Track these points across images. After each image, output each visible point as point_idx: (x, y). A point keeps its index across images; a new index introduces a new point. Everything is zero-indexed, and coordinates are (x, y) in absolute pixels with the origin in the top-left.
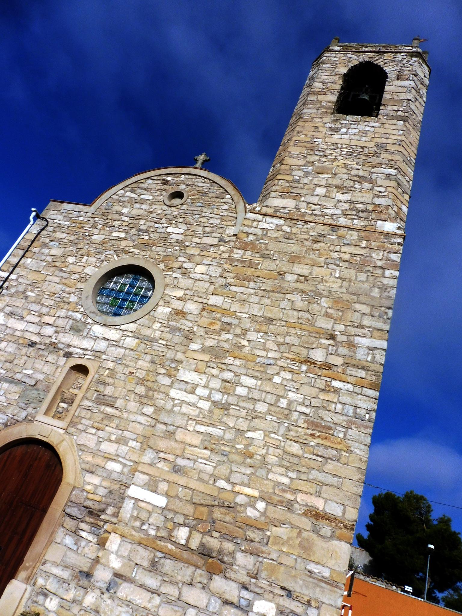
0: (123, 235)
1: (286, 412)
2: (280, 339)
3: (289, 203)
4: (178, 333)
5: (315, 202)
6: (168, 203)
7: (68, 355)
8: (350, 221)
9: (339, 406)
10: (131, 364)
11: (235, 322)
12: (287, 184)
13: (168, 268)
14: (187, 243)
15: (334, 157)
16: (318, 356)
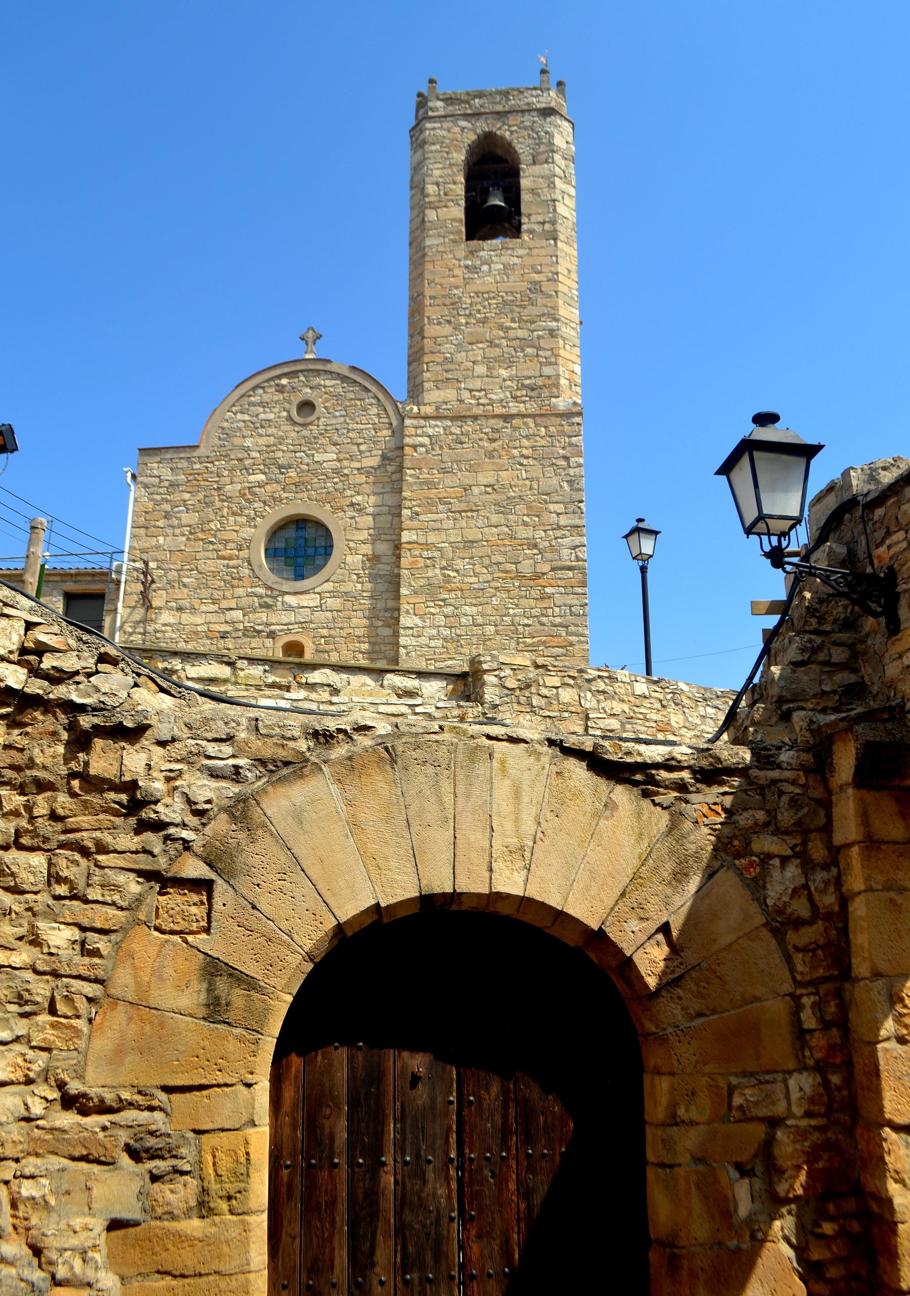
0: (262, 477)
1: (512, 628)
2: (487, 561)
3: (449, 394)
4: (379, 581)
5: (478, 387)
6: (298, 419)
7: (272, 635)
8: (522, 405)
9: (557, 610)
10: (346, 625)
11: (436, 554)
12: (439, 368)
13: (336, 509)
14: (346, 471)
15: (483, 315)
16: (526, 567)
